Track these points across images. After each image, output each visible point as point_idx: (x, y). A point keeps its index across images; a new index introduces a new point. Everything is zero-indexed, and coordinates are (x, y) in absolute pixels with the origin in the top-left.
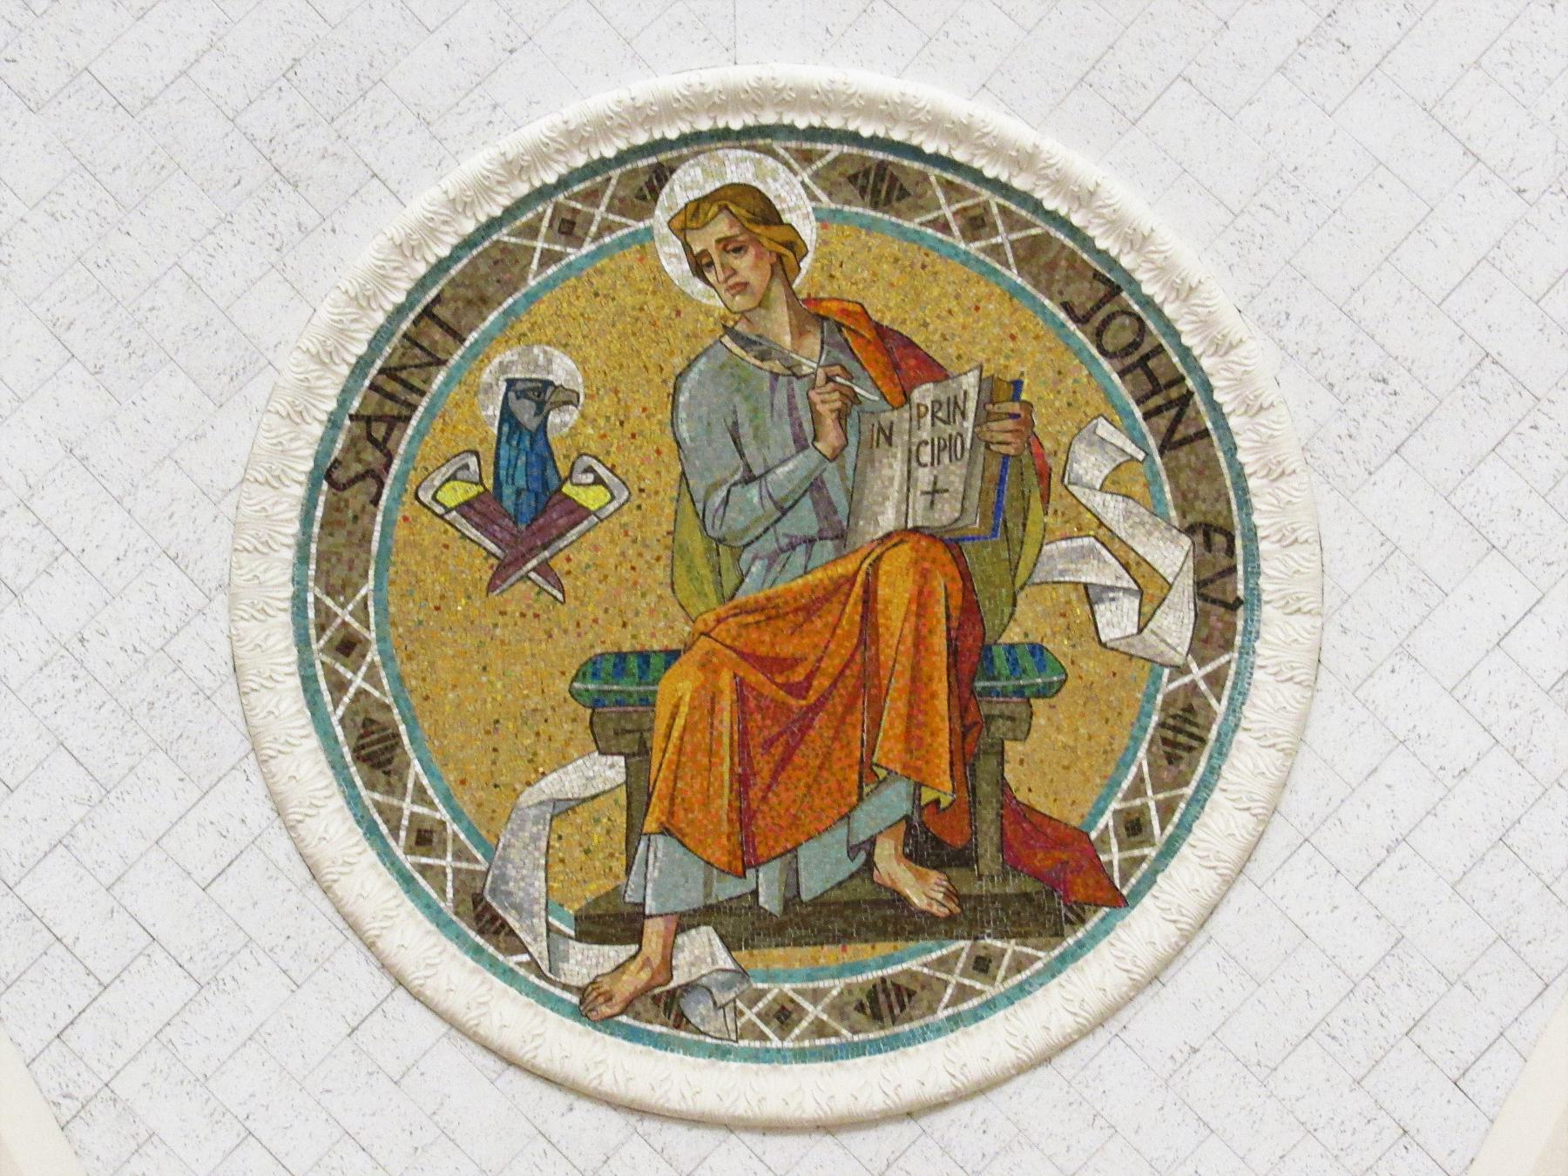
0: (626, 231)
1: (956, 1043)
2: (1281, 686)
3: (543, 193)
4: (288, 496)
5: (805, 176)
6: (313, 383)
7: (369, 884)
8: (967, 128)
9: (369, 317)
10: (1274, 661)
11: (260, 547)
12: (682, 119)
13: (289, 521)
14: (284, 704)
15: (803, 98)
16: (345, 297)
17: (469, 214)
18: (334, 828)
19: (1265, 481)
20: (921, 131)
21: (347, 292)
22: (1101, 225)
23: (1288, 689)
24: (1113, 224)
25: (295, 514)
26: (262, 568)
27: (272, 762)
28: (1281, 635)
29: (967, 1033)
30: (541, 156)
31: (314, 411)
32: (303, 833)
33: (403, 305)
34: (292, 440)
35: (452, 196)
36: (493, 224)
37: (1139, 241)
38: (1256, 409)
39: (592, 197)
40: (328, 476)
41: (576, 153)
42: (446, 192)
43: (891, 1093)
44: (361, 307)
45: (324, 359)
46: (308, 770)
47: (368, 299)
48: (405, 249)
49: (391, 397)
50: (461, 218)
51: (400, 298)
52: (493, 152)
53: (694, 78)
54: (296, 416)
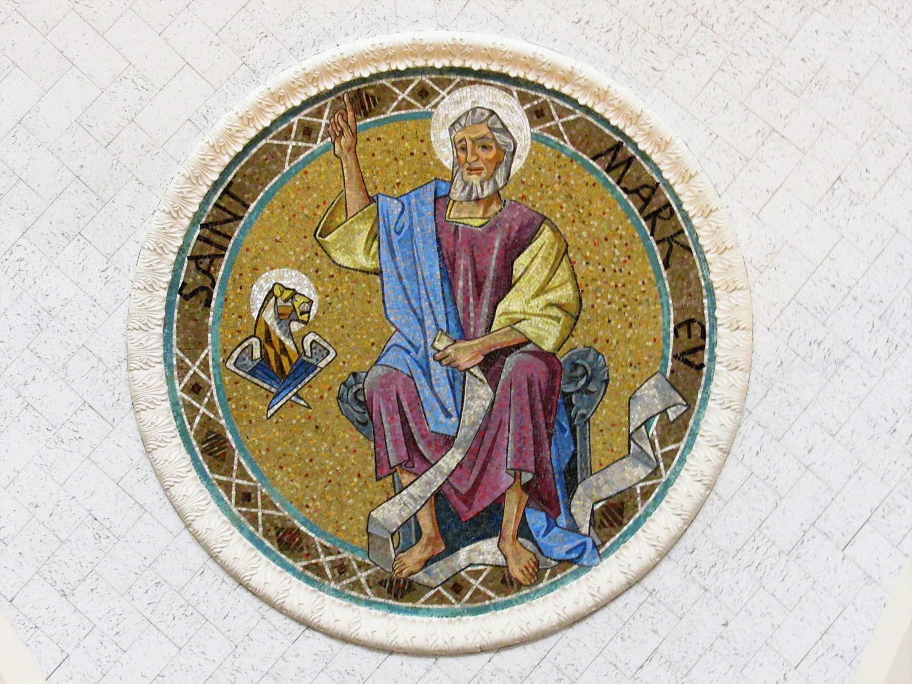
0: (309, 152)
1: (559, 595)
2: (731, 373)
3: (294, 111)
4: (155, 334)
5: (443, 93)
6: (186, 195)
7: (215, 522)
8: (533, 60)
9: (221, 159)
10: (726, 358)
11: (143, 327)
12: (370, 65)
13: (159, 311)
14: (162, 419)
15: (438, 51)
16: (183, 178)
17: (252, 125)
18: (192, 490)
19: (716, 255)
20: (509, 64)
21: (184, 175)
22: (613, 111)
23: (736, 374)
24: (619, 109)
25: (160, 343)
26: (144, 339)
27: (154, 452)
28: (729, 342)
29: (565, 589)
30: (291, 89)
31: (170, 247)
32: (173, 493)
33: (240, 153)
34: (158, 263)
35: (240, 115)
36: (265, 132)
37: (635, 118)
38: (708, 213)
39: (319, 113)
40: (180, 292)
41: (311, 88)
42: (184, 175)
43: (595, 593)
44: (175, 218)
45: (174, 214)
46: (176, 456)
47: (197, 178)
48: (216, 149)
49: (219, 233)
50: (248, 128)
51: (216, 177)
52: (263, 88)
53: (376, 41)
54: (159, 251)
